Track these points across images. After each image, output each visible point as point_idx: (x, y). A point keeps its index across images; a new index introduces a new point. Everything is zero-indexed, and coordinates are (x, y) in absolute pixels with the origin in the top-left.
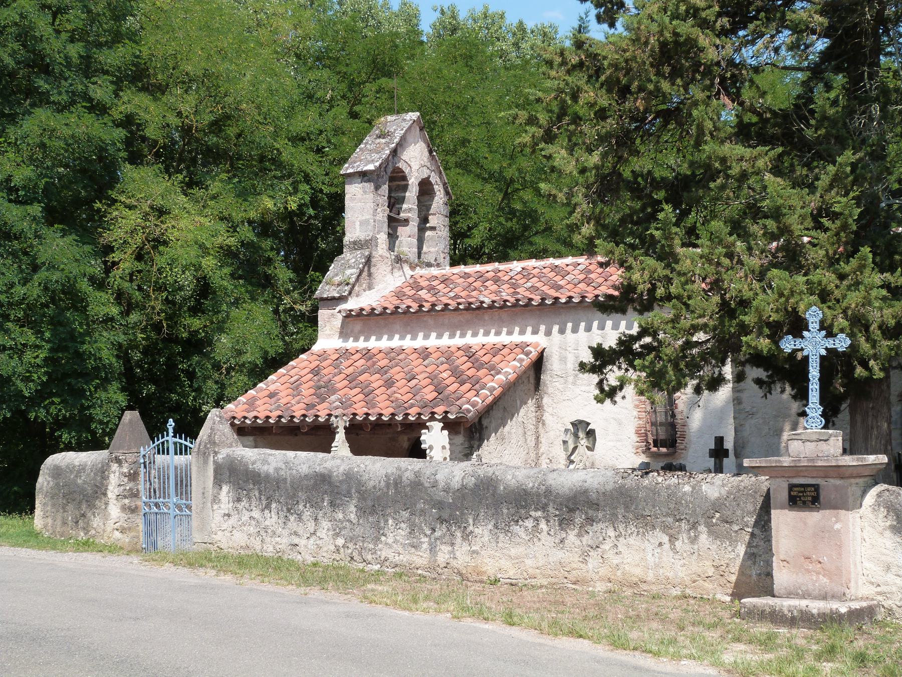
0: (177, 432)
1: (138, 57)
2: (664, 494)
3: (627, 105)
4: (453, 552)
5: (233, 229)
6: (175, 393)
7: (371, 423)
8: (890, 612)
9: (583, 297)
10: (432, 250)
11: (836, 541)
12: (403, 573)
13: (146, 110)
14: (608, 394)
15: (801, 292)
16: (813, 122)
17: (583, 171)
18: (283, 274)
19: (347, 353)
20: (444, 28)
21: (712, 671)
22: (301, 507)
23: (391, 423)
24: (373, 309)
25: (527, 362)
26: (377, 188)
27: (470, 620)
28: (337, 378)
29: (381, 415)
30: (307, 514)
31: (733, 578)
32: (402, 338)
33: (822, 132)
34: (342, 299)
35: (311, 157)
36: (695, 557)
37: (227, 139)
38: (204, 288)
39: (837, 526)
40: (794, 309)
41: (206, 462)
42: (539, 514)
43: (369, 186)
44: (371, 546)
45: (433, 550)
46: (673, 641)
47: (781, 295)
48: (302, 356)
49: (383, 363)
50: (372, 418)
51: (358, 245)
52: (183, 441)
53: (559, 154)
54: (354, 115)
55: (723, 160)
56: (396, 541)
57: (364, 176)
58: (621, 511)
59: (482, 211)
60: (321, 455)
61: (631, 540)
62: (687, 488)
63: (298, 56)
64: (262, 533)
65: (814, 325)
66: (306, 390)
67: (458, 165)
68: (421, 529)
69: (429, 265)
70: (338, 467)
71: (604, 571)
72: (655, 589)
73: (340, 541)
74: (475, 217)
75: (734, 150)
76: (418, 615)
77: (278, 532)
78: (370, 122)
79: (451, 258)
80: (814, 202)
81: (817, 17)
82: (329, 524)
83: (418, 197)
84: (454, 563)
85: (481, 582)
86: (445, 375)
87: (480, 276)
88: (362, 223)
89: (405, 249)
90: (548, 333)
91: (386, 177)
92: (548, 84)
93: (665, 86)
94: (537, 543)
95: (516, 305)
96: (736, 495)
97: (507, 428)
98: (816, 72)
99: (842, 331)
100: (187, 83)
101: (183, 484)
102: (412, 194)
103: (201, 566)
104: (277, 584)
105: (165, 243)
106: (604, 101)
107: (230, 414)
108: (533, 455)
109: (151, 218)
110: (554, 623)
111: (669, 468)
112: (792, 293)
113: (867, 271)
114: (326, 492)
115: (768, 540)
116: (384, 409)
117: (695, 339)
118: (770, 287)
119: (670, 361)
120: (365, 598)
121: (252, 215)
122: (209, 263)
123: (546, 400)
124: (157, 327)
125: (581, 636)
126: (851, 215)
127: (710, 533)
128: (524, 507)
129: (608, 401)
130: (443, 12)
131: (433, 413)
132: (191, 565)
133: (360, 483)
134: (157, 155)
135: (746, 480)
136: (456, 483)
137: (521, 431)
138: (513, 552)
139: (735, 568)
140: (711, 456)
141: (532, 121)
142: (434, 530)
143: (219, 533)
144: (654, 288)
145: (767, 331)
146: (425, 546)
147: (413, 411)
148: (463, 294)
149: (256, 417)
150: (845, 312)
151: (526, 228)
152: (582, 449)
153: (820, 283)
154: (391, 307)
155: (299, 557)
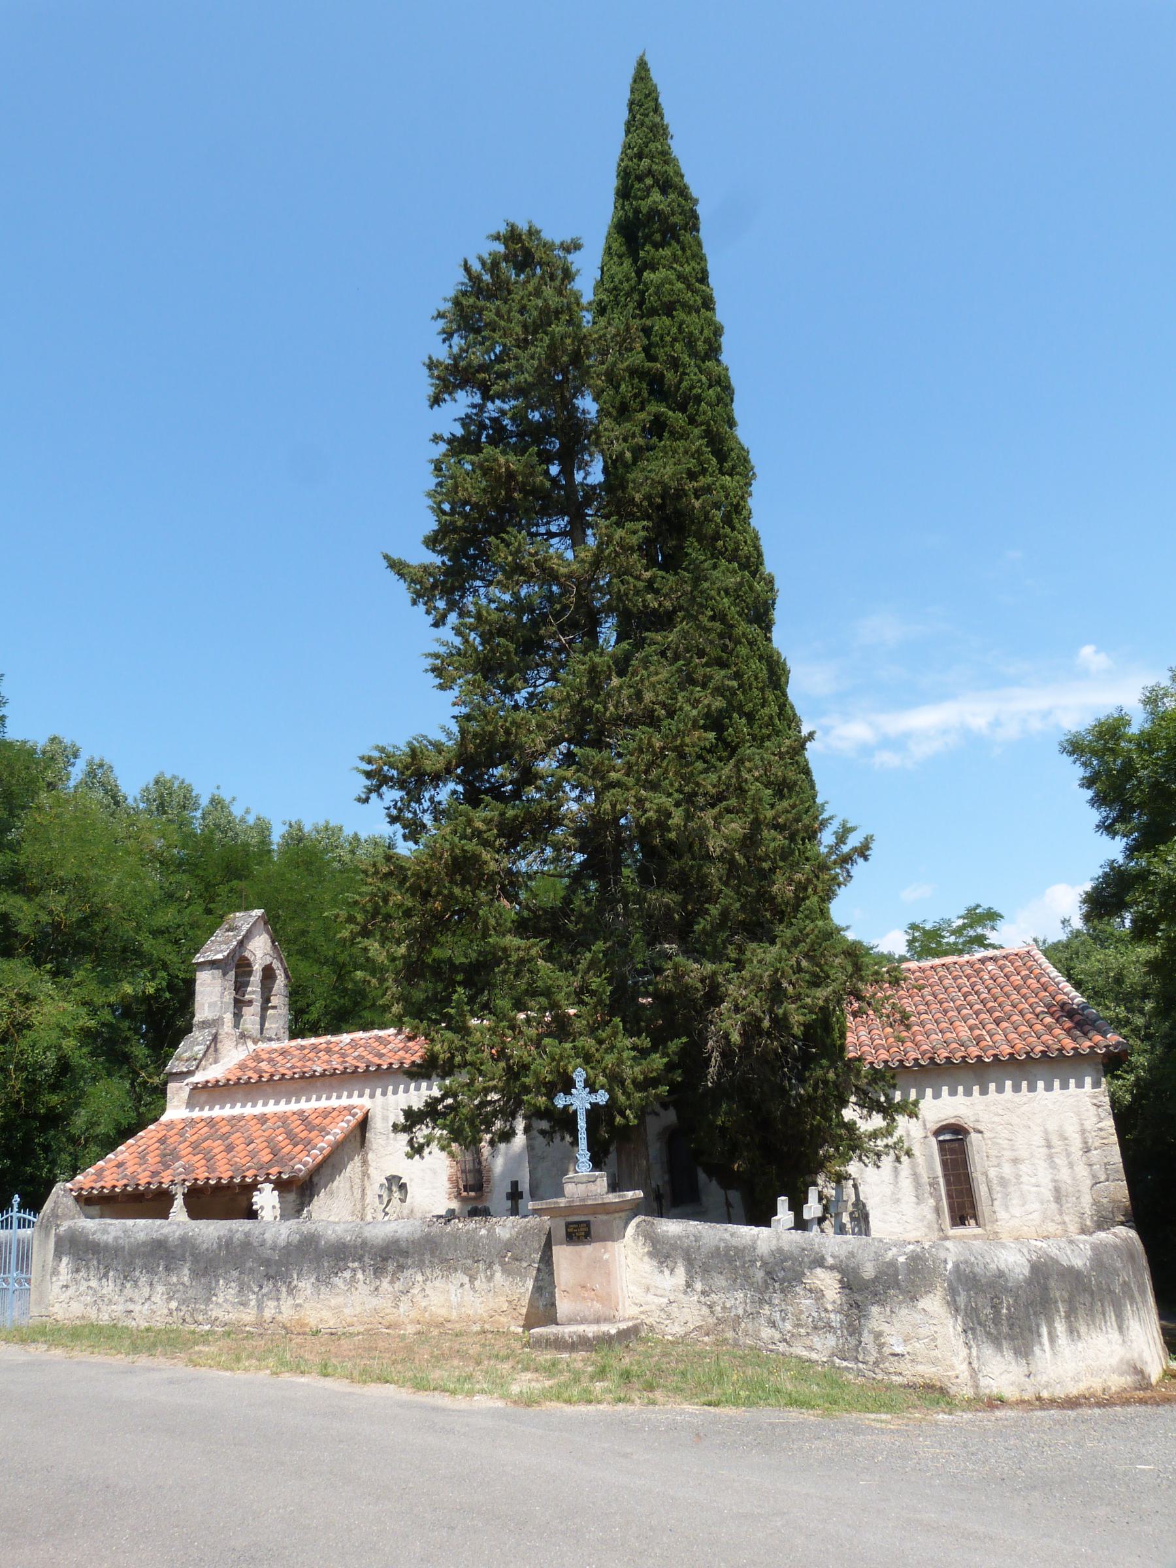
0: (22, 1207)
1: (16, 864)
2: (464, 1238)
3: (429, 905)
4: (278, 1307)
5: (94, 1012)
6: (30, 1166)
7: (212, 1186)
8: (651, 1328)
9: (402, 1063)
10: (273, 1026)
11: (604, 1268)
12: (232, 1331)
13: (20, 910)
14: (417, 1150)
15: (569, 1056)
16: (573, 918)
17: (393, 959)
18: (139, 1050)
19: (192, 1122)
20: (292, 838)
21: (500, 1404)
22: (137, 1273)
23: (230, 1186)
24: (218, 1081)
25: (354, 1122)
26: (225, 974)
27: (287, 1374)
28: (181, 1146)
29: (220, 1178)
30: (143, 1280)
31: (524, 1311)
32: (243, 1106)
33: (580, 926)
34: (190, 1073)
35: (169, 948)
36: (491, 1294)
37: (94, 933)
38: (64, 1066)
39: (606, 1256)
40: (564, 1070)
41: (47, 1235)
42: (356, 1264)
43: (218, 973)
44: (203, 1307)
45: (260, 1307)
46: (469, 1377)
47: (553, 1059)
48: (151, 1127)
49: (224, 1130)
50: (212, 1182)
51: (205, 1024)
52: (27, 1216)
53: (374, 947)
54: (209, 912)
55: (505, 950)
56: (226, 1301)
57: (213, 964)
58: (427, 1257)
59: (318, 990)
60: (158, 1222)
61: (437, 1283)
62: (483, 1232)
63: (161, 863)
64: (99, 1302)
65: (580, 1084)
66: (152, 1159)
67: (299, 952)
68: (249, 1287)
69: (270, 1039)
70: (174, 1232)
71: (414, 1314)
72: (458, 1327)
73: (174, 1305)
74: (312, 997)
75: (512, 941)
76: (240, 1375)
77: (114, 1300)
78: (222, 917)
79: (291, 1032)
80: (576, 982)
81: (570, 838)
82: (164, 1289)
83: (262, 982)
84: (279, 1318)
85: (304, 1333)
86: (280, 1138)
87: (314, 1047)
88: (210, 1005)
89: (249, 1026)
90: (372, 1096)
91: (233, 965)
92: (364, 889)
93: (457, 891)
94: (354, 1293)
95: (344, 1073)
96: (524, 1235)
97: (336, 1183)
98: (577, 878)
99: (602, 1087)
100: (61, 886)
101: (24, 1258)
102: (256, 978)
103: (34, 1341)
104: (106, 1354)
105: (29, 1027)
106: (409, 903)
107: (78, 1186)
108: (359, 1206)
109: (17, 1005)
110: (364, 1372)
111: (474, 1213)
112: (562, 1058)
113: (620, 1035)
114: (161, 1258)
115: (551, 1273)
116: (224, 1172)
117: (489, 1098)
118: (545, 1053)
119: (466, 1119)
120: (191, 1361)
121: (112, 999)
122: (69, 1044)
123: (370, 1156)
124: (16, 1104)
125: (387, 1382)
126: (604, 992)
127: (504, 1271)
128: (343, 1259)
129: (417, 1157)
130: (291, 826)
131: (268, 1174)
132: (23, 1341)
133: (194, 1247)
134: (28, 948)
135: (533, 1221)
136: (282, 1241)
137: (348, 1185)
138: (333, 1302)
139: (525, 1301)
140: (508, 1198)
141: (351, 919)
142: (261, 1287)
143: (57, 1305)
144: (453, 1056)
145: (543, 1090)
146: (253, 1303)
147: (250, 1173)
148: (299, 1064)
149: (103, 1187)
150: (604, 1071)
151: (356, 1004)
152: (395, 1201)
153: (583, 1048)
154: (234, 1079)
155: (134, 1323)
